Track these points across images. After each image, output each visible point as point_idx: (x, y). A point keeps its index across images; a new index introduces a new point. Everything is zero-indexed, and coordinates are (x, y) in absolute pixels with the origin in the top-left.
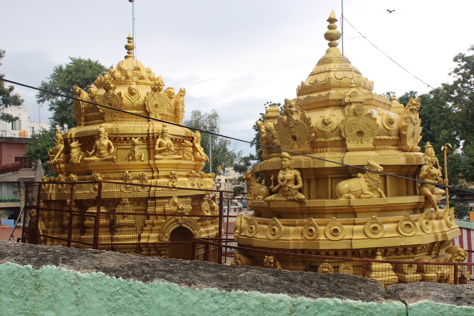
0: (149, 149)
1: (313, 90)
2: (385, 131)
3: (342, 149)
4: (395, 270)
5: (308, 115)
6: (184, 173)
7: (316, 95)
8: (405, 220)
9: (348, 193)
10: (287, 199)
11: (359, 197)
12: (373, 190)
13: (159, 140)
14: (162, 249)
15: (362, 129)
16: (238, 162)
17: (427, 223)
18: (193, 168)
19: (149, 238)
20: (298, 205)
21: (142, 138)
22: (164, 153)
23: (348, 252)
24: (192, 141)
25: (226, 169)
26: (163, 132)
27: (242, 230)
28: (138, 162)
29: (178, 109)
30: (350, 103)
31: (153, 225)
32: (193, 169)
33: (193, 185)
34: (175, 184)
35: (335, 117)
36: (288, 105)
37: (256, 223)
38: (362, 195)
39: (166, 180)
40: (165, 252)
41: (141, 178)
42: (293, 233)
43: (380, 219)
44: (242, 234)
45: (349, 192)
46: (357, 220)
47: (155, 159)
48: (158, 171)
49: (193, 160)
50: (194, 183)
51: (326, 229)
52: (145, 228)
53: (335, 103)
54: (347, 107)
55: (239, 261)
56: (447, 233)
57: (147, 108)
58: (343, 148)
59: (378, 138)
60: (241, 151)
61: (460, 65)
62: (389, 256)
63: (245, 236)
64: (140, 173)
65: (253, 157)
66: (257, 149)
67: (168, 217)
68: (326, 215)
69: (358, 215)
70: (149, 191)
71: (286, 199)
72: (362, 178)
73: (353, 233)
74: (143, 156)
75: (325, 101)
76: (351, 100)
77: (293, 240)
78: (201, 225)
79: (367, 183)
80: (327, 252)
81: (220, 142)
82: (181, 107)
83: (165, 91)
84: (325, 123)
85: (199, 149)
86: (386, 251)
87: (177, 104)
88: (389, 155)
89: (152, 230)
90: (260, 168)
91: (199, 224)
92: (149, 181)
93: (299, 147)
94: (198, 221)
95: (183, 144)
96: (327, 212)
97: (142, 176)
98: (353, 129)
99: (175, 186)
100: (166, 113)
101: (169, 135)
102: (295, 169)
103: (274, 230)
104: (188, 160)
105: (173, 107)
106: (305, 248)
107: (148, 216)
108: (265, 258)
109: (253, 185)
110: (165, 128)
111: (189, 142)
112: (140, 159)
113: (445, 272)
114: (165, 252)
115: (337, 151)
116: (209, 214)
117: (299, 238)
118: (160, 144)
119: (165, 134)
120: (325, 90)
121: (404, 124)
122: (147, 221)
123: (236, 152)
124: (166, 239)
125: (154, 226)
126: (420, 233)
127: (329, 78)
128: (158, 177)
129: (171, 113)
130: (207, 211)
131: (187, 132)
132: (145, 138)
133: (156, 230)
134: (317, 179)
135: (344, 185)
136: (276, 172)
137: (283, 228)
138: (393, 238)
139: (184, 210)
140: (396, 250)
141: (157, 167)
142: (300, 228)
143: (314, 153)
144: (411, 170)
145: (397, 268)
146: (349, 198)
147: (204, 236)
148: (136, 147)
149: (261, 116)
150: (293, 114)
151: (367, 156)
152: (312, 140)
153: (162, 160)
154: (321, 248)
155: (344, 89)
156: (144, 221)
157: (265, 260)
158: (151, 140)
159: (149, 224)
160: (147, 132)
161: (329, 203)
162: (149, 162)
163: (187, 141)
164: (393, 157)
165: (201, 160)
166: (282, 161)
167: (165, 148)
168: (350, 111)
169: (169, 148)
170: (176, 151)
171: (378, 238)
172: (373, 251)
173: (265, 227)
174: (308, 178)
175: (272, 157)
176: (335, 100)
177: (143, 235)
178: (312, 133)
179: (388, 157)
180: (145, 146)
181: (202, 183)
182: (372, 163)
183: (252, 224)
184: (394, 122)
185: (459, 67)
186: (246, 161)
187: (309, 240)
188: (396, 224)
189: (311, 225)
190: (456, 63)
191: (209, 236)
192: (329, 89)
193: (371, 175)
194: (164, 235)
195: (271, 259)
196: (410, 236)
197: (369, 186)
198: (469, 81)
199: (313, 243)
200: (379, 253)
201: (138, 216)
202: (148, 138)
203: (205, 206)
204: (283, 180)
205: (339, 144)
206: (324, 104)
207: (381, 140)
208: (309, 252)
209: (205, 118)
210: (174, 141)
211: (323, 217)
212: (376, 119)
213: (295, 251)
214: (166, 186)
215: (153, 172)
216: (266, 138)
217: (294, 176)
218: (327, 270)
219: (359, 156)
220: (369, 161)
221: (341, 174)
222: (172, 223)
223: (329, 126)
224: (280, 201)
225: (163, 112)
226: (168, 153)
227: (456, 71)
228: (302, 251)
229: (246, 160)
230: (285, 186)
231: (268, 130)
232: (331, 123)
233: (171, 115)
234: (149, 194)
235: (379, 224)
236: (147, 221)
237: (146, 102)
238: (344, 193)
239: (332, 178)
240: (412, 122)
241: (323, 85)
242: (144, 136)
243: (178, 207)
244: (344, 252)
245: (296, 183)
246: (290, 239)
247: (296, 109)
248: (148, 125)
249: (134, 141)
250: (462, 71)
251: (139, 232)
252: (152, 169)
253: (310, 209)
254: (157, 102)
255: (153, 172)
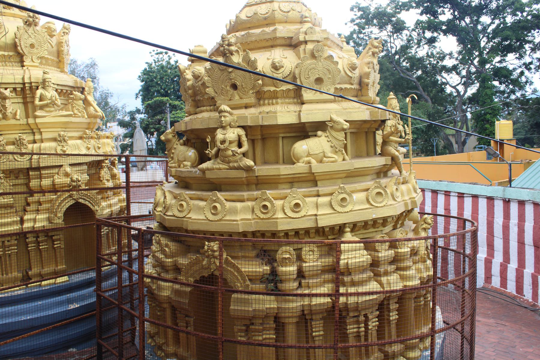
0: (25, 103)
1: (252, 25)
2: (347, 79)
3: (295, 100)
4: (366, 249)
5: (253, 56)
6: (76, 134)
7: (258, 31)
8: (376, 187)
9: (307, 156)
10: (229, 166)
11: (321, 161)
12: (336, 152)
13: (39, 92)
14: (53, 233)
15: (321, 76)
16: (121, 116)
17: (397, 189)
18: (86, 126)
19: (35, 220)
20: (244, 174)
21: (15, 89)
22: (48, 109)
23: (311, 231)
24: (82, 93)
25: (108, 125)
26: (44, 81)
27: (168, 208)
28: (13, 122)
29: (63, 51)
30: (306, 42)
31: (40, 203)
32: (87, 129)
33: (89, 149)
34: (65, 149)
35: (287, 60)
36: (227, 42)
37: (188, 199)
38: (325, 159)
39: (53, 144)
40: (58, 237)
41: (18, 143)
42: (241, 210)
43: (348, 187)
44: (168, 214)
45: (309, 155)
46: (322, 190)
47: (35, 117)
48: (41, 133)
49: (86, 117)
50: (89, 146)
51: (285, 205)
52: (28, 208)
53: (283, 42)
54: (302, 47)
55: (167, 249)
56: (416, 199)
57: (19, 48)
58: (297, 99)
59: (338, 86)
60: (125, 104)
61: (356, 15)
62: (357, 231)
63: (174, 216)
64: (17, 136)
65: (140, 110)
66: (142, 102)
67: (59, 193)
68: (279, 185)
69: (319, 183)
70: (31, 159)
71: (227, 167)
72: (323, 138)
73: (317, 207)
74: (18, 113)
75: (271, 39)
76: (307, 38)
77: (242, 220)
78: (102, 198)
79: (330, 144)
80: (286, 234)
81: (101, 95)
82: (65, 48)
83: (43, 27)
84: (275, 67)
85: (92, 103)
86: (354, 227)
87: (60, 44)
88: (352, 109)
89: (38, 210)
90: (186, 126)
91: (100, 197)
92: (30, 146)
93: (241, 98)
94: (97, 193)
95: (72, 96)
96: (281, 181)
97: (20, 139)
98: (310, 75)
99: (64, 151)
100: (46, 56)
101: (52, 85)
102: (239, 127)
103: (215, 208)
104: (79, 117)
105: (55, 49)
106: (258, 229)
107: (31, 193)
108: (204, 244)
109: (175, 148)
110: (46, 76)
111: (79, 94)
112: (14, 117)
113: (415, 245)
114: (58, 237)
115: (289, 103)
116: (110, 184)
117: (250, 217)
118: (40, 97)
119: (47, 83)
120: (267, 25)
121: (366, 70)
122: (30, 199)
123: (119, 106)
124: (59, 221)
125: (41, 205)
126: (392, 202)
127: (273, 11)
128: (42, 141)
129: (53, 56)
130: (108, 180)
131: (76, 82)
132: (18, 89)
133: (43, 210)
134: (264, 139)
135: (301, 147)
136: (212, 131)
137: (228, 204)
138: (364, 211)
139: (79, 181)
140: (366, 225)
141: (39, 127)
142: (250, 204)
143: (260, 105)
144: (372, 126)
145: (369, 245)
146: (309, 163)
147: (107, 211)
148: (7, 101)
149: (147, 65)
150: (232, 54)
151: (328, 109)
152: (258, 89)
153: (45, 118)
154: (280, 228)
155: (291, 24)
156: (26, 199)
157: (206, 247)
158: (28, 92)
159: (33, 202)
160: (21, 81)
161: (284, 170)
162: (27, 121)
163: (77, 93)
164: (357, 110)
165: (95, 117)
166: (221, 117)
167: (49, 101)
168: (307, 51)
169: (54, 102)
170: (62, 106)
171: (348, 212)
172: (340, 227)
173: (202, 204)
174: (253, 138)
175: (202, 112)
176: (284, 38)
177: (26, 217)
178: (259, 80)
179: (351, 110)
180: (20, 100)
181: (100, 146)
182: (335, 117)
183: (182, 200)
184: (356, 68)
185: (355, 17)
186: (132, 115)
187: (263, 219)
188: (365, 193)
189: (265, 200)
190: (353, 13)
191: (112, 211)
192: (273, 24)
193: (334, 133)
194: (56, 215)
195: (215, 246)
196: (382, 207)
197: (332, 147)
198: (363, 31)
199: (268, 222)
200: (348, 229)
201: (20, 195)
202: (23, 89)
203: (105, 173)
204: (223, 142)
205: (292, 94)
206: (270, 43)
207: (342, 89)
208: (263, 234)
209: (82, 67)
210: (60, 93)
211: (276, 188)
212: (337, 63)
213: (244, 234)
214: (54, 152)
215: (34, 133)
216: (193, 87)
217: (237, 136)
218: (288, 256)
219: (319, 110)
220: (332, 116)
221: (295, 132)
222: (65, 199)
223: (281, 71)
224: (220, 169)
225: (42, 54)
226: (53, 109)
227: (352, 21)
228: (254, 234)
229: (132, 114)
230: (226, 149)
231: (196, 77)
232: (283, 67)
233: (52, 58)
234: (31, 162)
235: (348, 194)
236: (30, 199)
237: (17, 40)
238: (302, 157)
239: (283, 137)
240: (373, 67)
241: (265, 19)
242: (17, 86)
243: (71, 178)
244: (307, 231)
245: (240, 146)
246: (238, 219)
247: (236, 48)
248: (22, 72)
249: (4, 94)
250: (358, 21)
251: (20, 214)
252: (32, 130)
253: (259, 178)
254: (33, 41)
255: (34, 133)
